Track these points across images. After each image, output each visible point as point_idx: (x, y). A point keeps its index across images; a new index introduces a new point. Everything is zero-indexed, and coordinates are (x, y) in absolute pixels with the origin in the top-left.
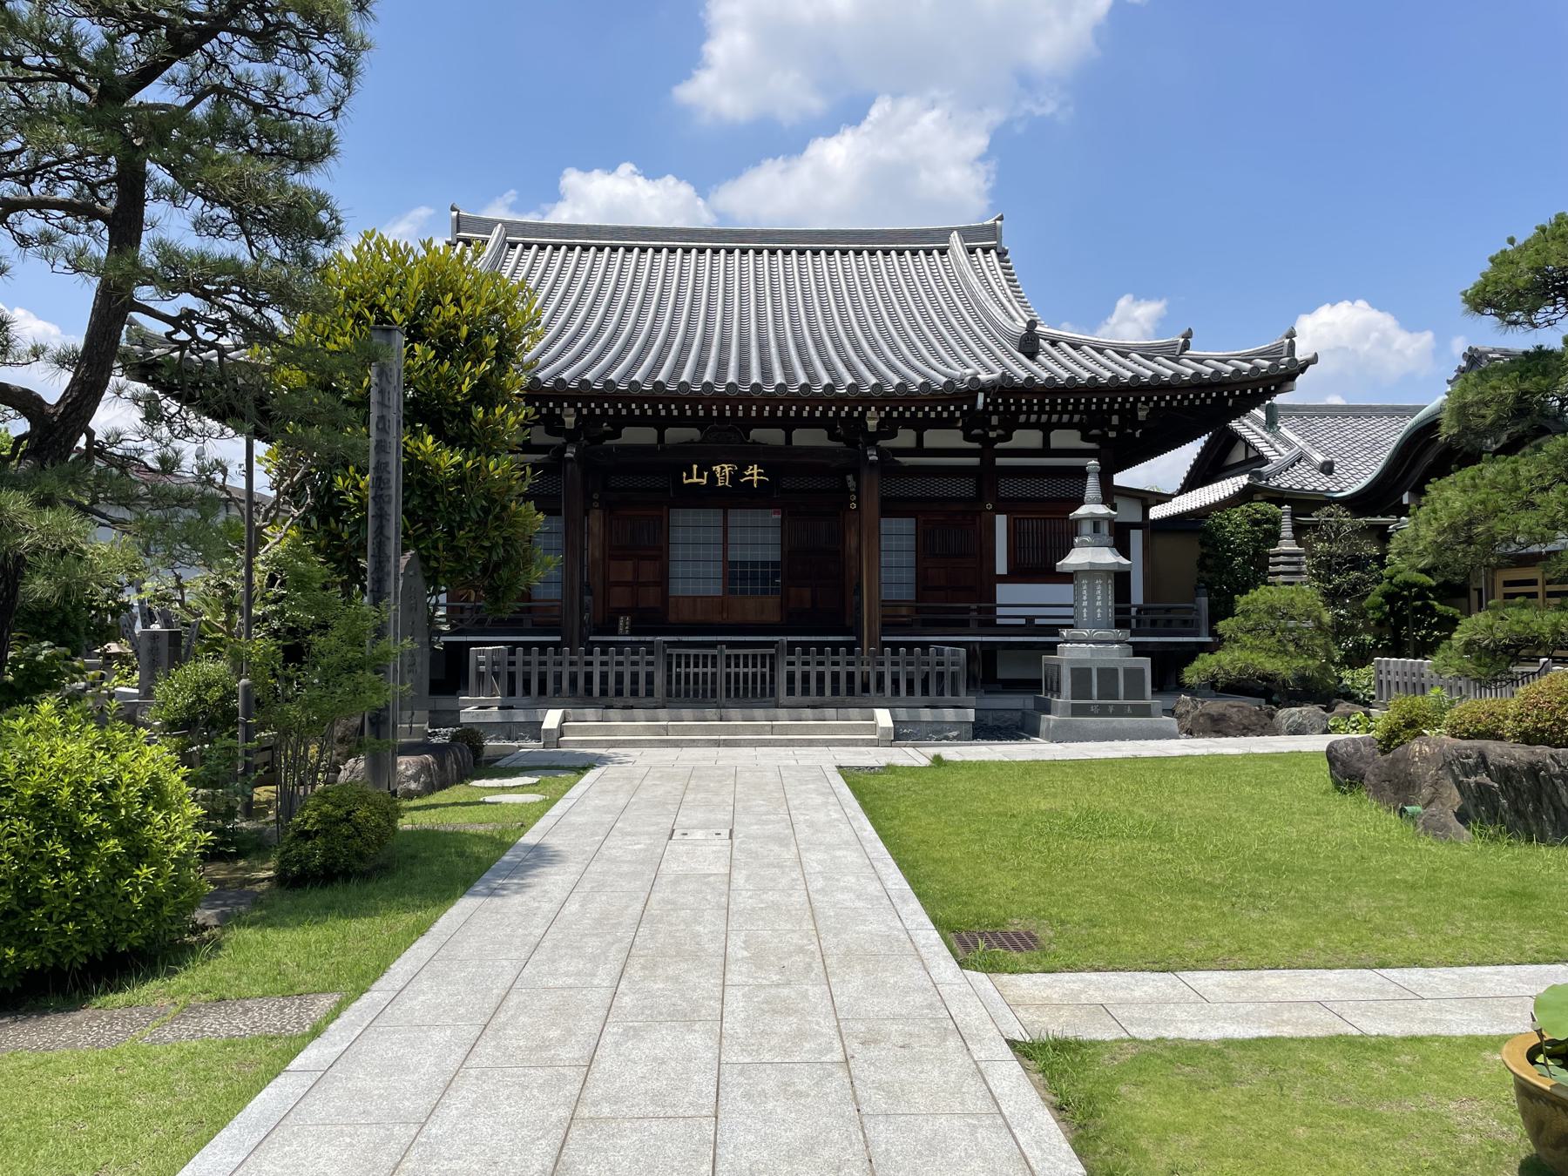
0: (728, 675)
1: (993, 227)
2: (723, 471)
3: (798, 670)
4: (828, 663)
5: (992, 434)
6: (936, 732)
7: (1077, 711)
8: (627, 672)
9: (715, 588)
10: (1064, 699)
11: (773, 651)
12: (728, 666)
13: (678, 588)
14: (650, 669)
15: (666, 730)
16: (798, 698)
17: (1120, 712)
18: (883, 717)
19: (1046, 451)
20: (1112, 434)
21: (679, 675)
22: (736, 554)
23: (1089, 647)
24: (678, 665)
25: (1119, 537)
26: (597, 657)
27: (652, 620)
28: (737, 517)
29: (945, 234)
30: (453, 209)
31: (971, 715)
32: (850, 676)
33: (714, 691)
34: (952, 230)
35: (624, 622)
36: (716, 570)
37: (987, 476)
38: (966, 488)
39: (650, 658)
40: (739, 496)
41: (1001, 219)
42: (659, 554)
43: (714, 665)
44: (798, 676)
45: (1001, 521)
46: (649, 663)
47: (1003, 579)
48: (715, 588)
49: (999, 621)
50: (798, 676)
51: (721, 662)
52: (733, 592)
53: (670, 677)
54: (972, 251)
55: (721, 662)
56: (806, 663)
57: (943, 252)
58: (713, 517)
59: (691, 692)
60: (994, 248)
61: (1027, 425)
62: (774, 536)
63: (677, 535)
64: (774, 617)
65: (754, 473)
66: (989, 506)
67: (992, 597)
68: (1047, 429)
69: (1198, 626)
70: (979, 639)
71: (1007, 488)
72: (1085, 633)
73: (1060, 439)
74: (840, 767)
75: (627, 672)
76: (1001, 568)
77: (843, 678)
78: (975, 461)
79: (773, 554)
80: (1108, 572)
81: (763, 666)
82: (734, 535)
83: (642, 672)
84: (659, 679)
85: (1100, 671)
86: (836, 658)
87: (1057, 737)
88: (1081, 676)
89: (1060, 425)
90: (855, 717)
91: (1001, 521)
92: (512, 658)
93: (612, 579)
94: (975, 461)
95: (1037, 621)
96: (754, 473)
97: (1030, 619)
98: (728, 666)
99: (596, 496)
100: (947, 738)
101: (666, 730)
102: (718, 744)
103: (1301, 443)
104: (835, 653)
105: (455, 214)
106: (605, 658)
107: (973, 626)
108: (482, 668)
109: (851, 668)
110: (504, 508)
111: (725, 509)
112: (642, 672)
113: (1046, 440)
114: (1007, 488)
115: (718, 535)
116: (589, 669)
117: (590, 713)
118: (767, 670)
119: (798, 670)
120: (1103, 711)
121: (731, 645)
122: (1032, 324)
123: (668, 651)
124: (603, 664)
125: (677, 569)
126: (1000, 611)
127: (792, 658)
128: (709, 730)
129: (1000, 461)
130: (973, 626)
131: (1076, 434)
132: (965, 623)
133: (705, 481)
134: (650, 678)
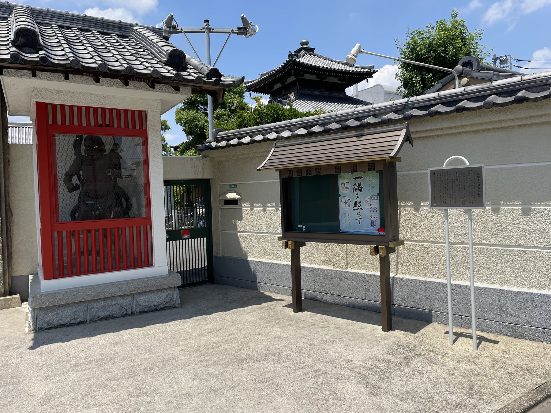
122: (252, 209)
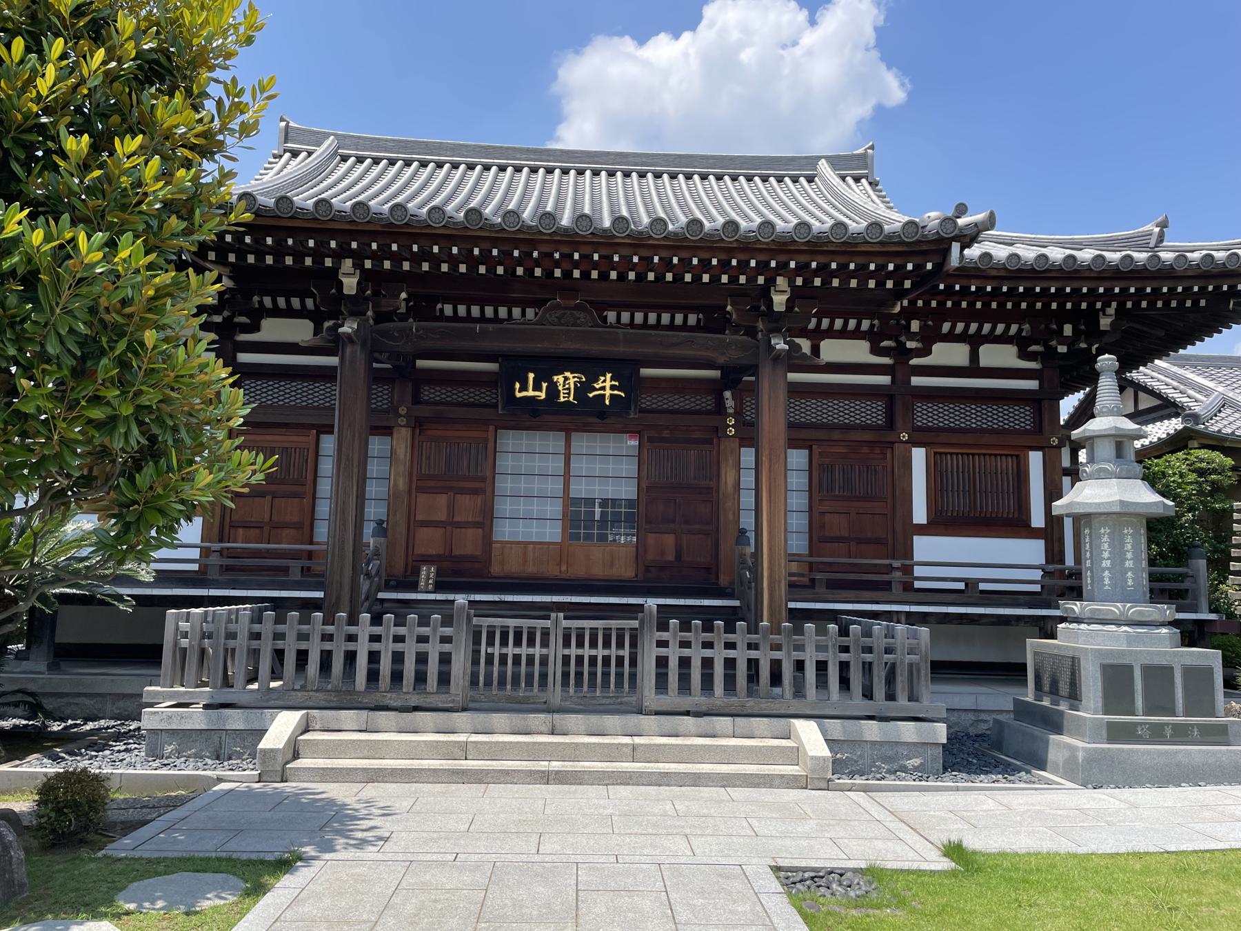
0: (566, 659)
1: (864, 156)
2: (567, 382)
3: (674, 654)
4: (719, 646)
5: (911, 345)
6: (886, 759)
7: (1117, 733)
8: (410, 650)
9: (552, 532)
10: (1090, 711)
11: (635, 624)
12: (567, 644)
13: (505, 531)
14: (447, 647)
15: (464, 751)
16: (672, 698)
17: (1181, 734)
18: (810, 737)
19: (974, 370)
20: (1062, 349)
21: (490, 658)
22: (580, 489)
23: (1112, 628)
24: (491, 643)
25: (1148, 464)
26: (365, 627)
27: (460, 574)
28: (581, 443)
29: (813, 161)
30: (282, 120)
31: (940, 732)
32: (753, 664)
33: (544, 676)
34: (820, 158)
35: (427, 574)
36: (554, 508)
37: (898, 399)
38: (873, 413)
39: (447, 631)
40: (586, 416)
41: (872, 148)
42: (480, 485)
43: (545, 644)
44: (673, 664)
45: (919, 456)
46: (446, 640)
47: (922, 530)
48: (552, 532)
49: (917, 584)
50: (673, 664)
51: (556, 640)
52: (576, 537)
53: (476, 653)
54: (843, 178)
55: (556, 640)
56: (685, 644)
57: (810, 180)
58: (553, 442)
59: (506, 687)
60: (866, 177)
61: (951, 338)
62: (629, 468)
63: (506, 462)
64: (625, 570)
65: (606, 385)
66: (905, 437)
67: (909, 553)
68: (975, 342)
69: (1196, 598)
70: (906, 608)
71: (925, 415)
72: (1115, 609)
73: (992, 355)
74: (777, 869)
75: (410, 650)
76: (920, 515)
77: (742, 668)
78: (885, 380)
79: (628, 491)
80: (1138, 515)
81: (620, 645)
82: (578, 466)
83: (434, 650)
84: (460, 666)
85: (1148, 670)
86: (731, 637)
87: (1095, 775)
88: (1117, 679)
89: (993, 339)
90: (760, 736)
91: (919, 456)
92: (257, 628)
93: (419, 517)
94: (885, 380)
95: (982, 586)
96: (606, 385)
97: (971, 584)
98: (567, 644)
99: (403, 410)
100: (904, 769)
101: (464, 751)
102: (546, 778)
103: (1221, 389)
104: (708, 628)
105: (283, 124)
106: (377, 630)
107: (897, 590)
108: (184, 642)
109: (754, 654)
110: (137, 346)
111: (568, 432)
112: (434, 650)
113: (974, 356)
114: (925, 415)
115: (557, 464)
116: (351, 646)
117: (348, 717)
118: (626, 653)
119: (674, 654)
120: (1157, 735)
121: (574, 611)
123: (475, 621)
124: (375, 638)
125: (504, 507)
126: (918, 571)
127: (664, 636)
128: (533, 752)
129: (916, 381)
130: (897, 590)
131: (1012, 350)
132: (886, 586)
133: (543, 395)
134: (445, 659)
